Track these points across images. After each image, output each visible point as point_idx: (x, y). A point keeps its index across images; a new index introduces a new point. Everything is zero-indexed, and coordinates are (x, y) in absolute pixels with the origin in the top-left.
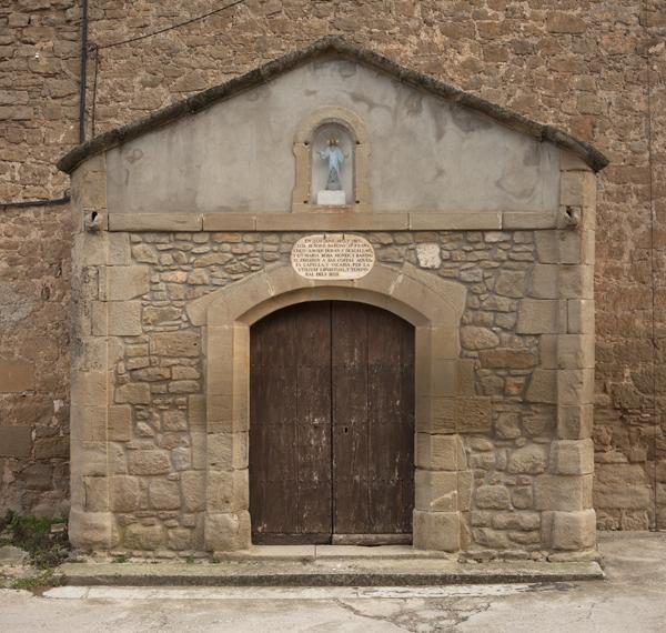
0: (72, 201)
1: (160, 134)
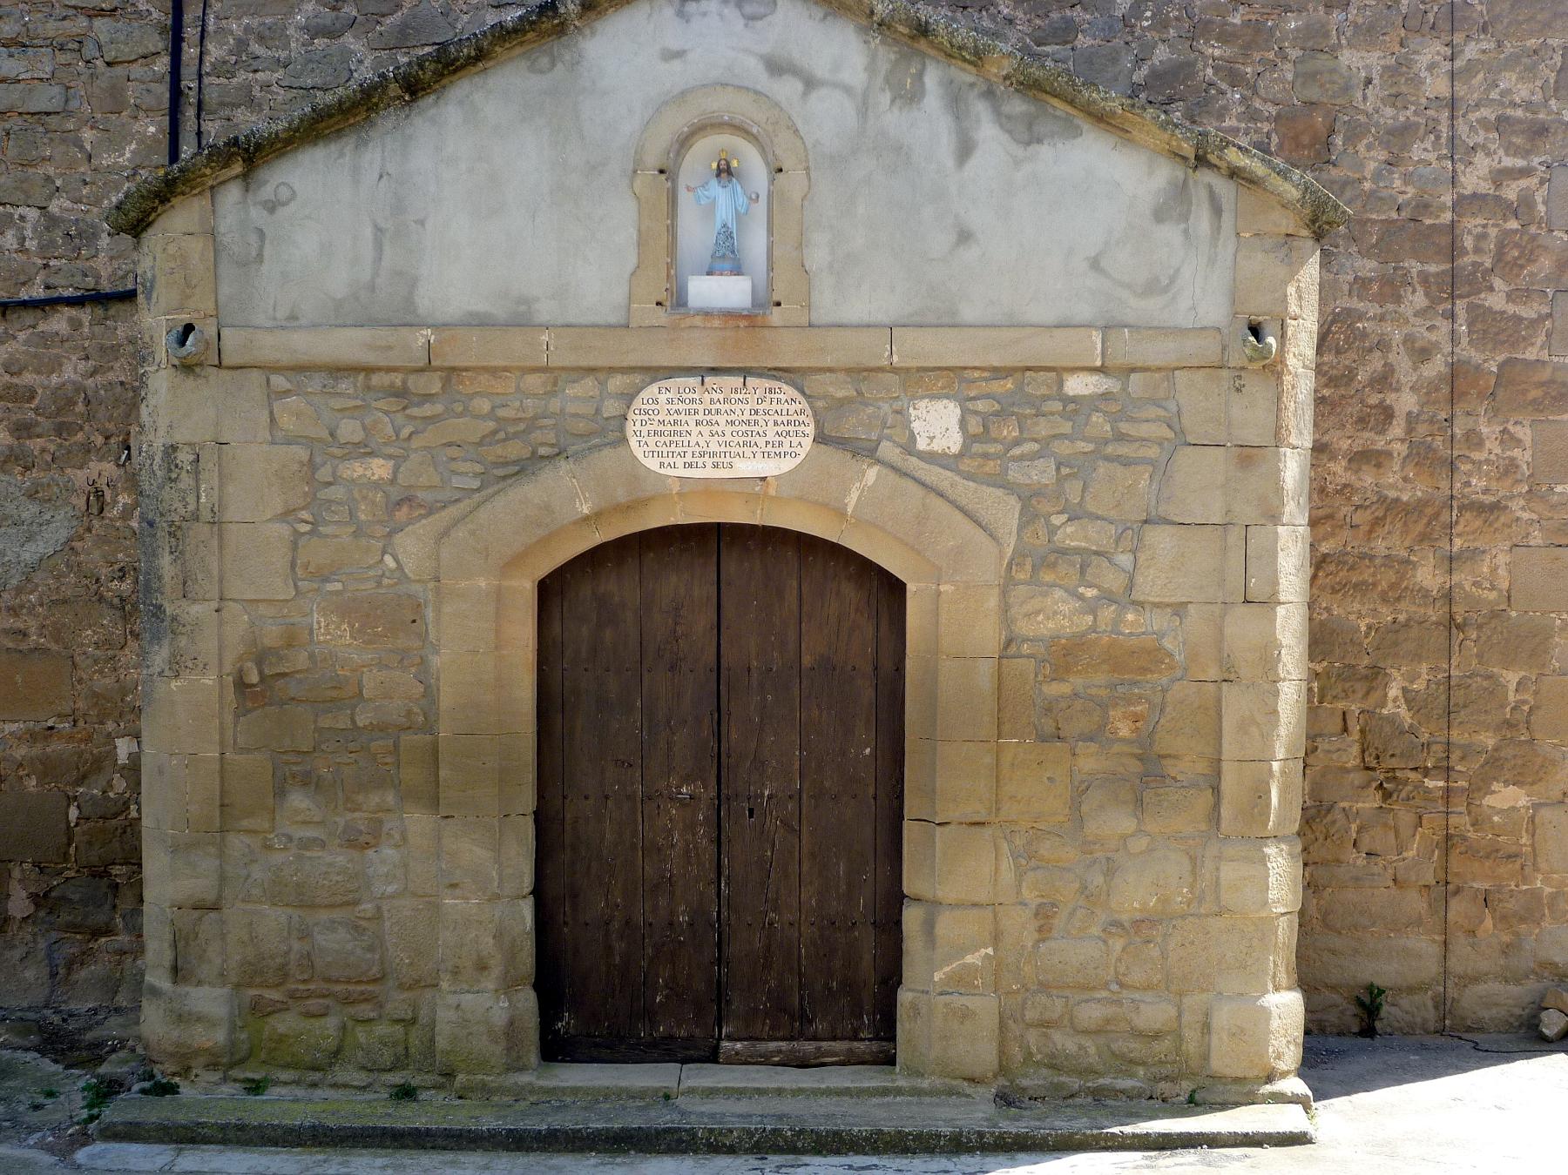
0: (141, 298)
1: (334, 147)
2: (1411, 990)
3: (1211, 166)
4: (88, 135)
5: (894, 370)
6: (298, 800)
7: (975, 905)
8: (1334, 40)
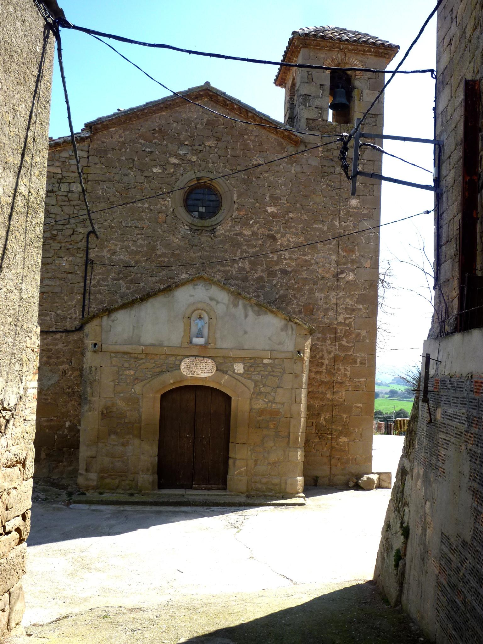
1: (126, 310)
2: (324, 477)
3: (292, 321)
4: (66, 298)
5: (231, 357)
6: (113, 437)
7: (243, 459)
8: (315, 291)
